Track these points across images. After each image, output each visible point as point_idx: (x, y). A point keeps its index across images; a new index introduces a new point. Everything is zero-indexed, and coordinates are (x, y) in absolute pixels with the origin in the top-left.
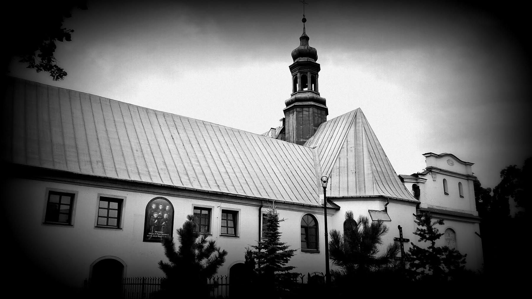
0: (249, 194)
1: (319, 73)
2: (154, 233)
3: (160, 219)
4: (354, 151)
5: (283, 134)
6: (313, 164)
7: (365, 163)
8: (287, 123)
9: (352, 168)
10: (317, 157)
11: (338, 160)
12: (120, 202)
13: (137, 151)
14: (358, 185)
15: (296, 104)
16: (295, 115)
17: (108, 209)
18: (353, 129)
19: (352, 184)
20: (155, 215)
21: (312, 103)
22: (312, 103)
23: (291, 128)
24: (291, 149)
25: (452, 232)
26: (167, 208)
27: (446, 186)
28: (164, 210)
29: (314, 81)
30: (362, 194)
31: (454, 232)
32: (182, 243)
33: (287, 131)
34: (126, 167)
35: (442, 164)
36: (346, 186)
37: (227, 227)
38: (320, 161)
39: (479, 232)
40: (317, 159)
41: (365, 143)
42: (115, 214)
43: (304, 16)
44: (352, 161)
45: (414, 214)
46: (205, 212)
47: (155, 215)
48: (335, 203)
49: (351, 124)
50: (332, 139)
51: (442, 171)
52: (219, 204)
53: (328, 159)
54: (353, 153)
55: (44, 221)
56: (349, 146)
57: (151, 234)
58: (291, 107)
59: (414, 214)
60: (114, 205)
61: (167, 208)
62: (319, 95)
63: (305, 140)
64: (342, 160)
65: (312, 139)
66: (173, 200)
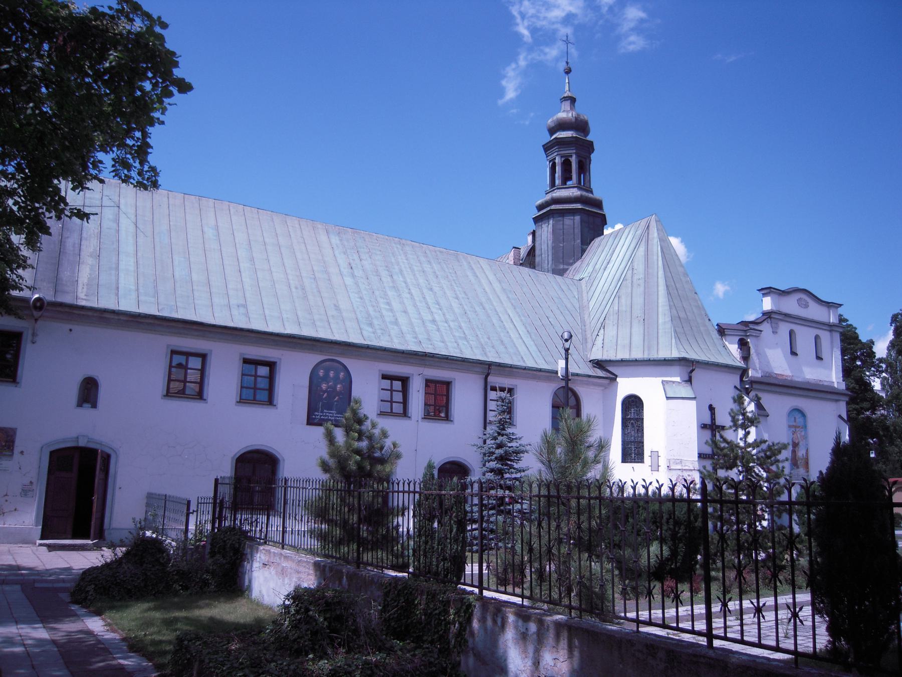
0: (468, 354)
1: (593, 156)
2: (322, 412)
3: (332, 392)
4: (642, 285)
5: (530, 260)
6: (577, 306)
7: (660, 305)
8: (538, 239)
9: (638, 311)
10: (585, 294)
11: (617, 299)
12: (272, 365)
13: (296, 288)
14: (646, 343)
15: (553, 207)
16: (551, 226)
17: (256, 376)
18: (642, 250)
19: (637, 339)
20: (324, 386)
21: (579, 206)
22: (579, 206)
23: (544, 247)
24: (542, 282)
25: (800, 415)
26: (342, 375)
27: (793, 341)
28: (336, 379)
29: (584, 168)
30: (654, 356)
31: (803, 415)
32: (636, 500)
33: (537, 252)
34: (281, 313)
35: (790, 305)
36: (628, 341)
37: (391, 402)
38: (589, 301)
39: (845, 416)
40: (585, 298)
41: (661, 272)
42: (263, 384)
43: (567, 63)
44: (639, 300)
45: (735, 387)
46: (192, 388)
47: (324, 386)
48: (610, 369)
49: (640, 240)
50: (610, 265)
51: (787, 317)
52: (420, 370)
53: (601, 298)
54: (642, 288)
55: (165, 392)
56: (636, 277)
57: (318, 415)
58: (547, 213)
59: (735, 387)
60: (263, 371)
61: (342, 375)
62: (591, 192)
63: (566, 267)
64: (623, 301)
65: (578, 264)
66: (352, 364)
